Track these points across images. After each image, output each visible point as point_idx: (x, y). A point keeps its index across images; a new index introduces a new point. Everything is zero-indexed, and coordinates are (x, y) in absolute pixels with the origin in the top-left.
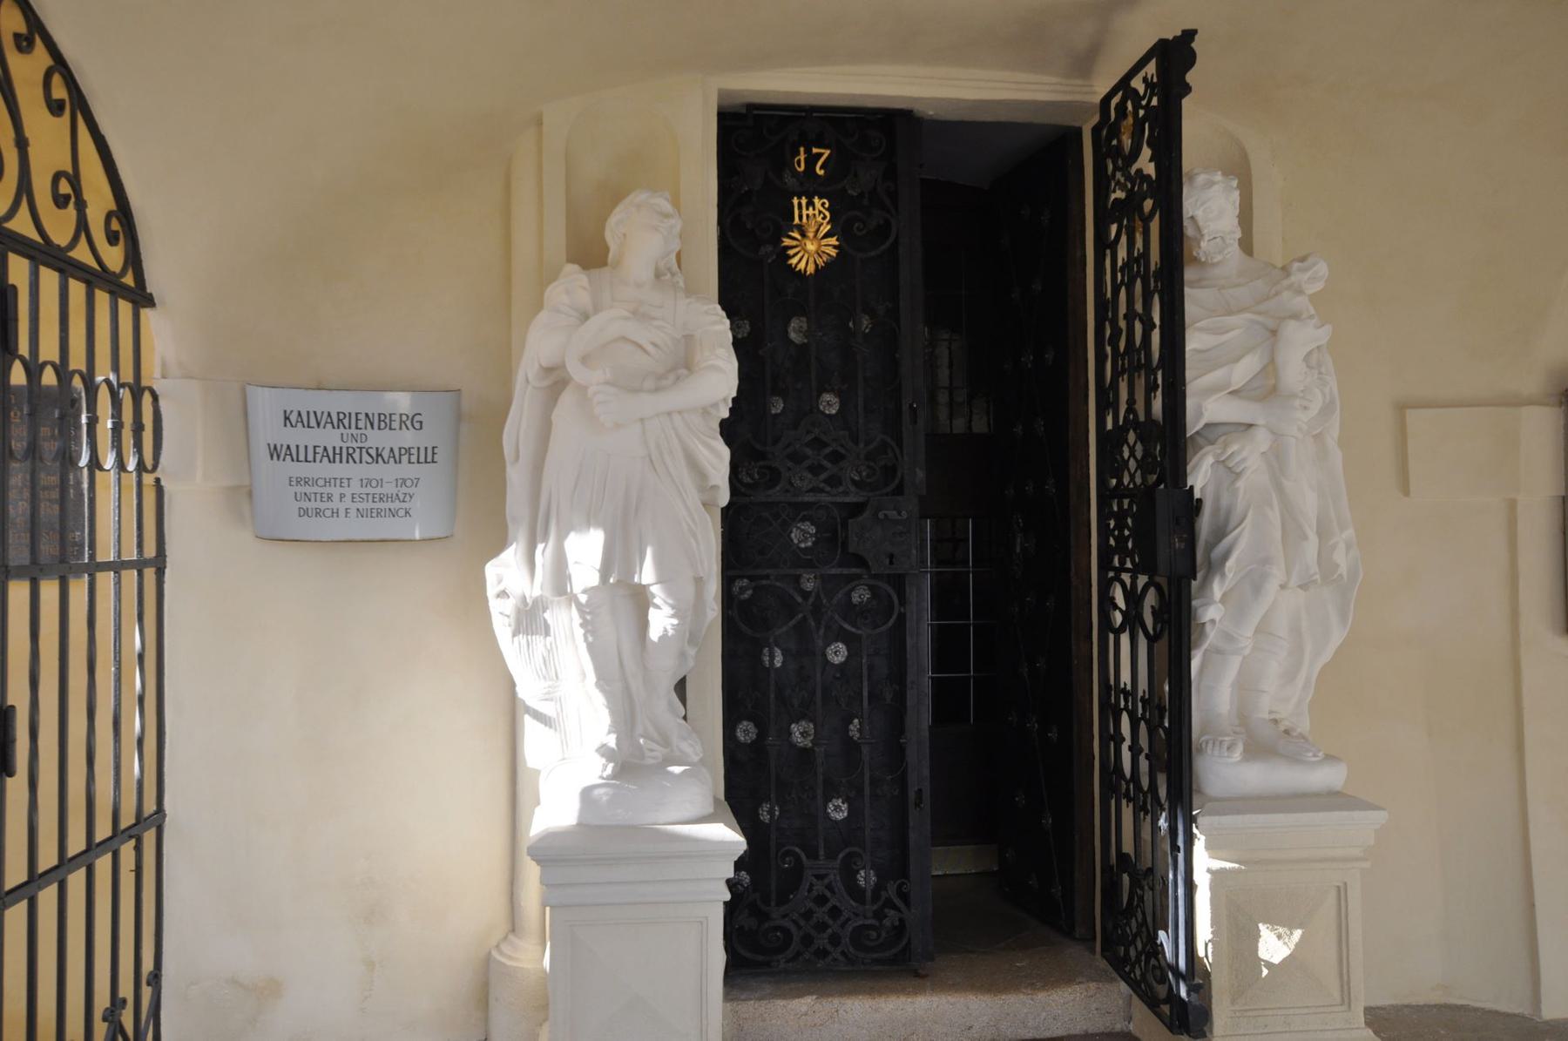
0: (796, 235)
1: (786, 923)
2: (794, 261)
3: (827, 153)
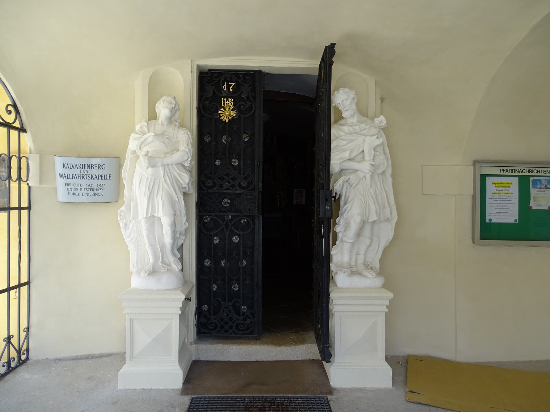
2: (222, 118)
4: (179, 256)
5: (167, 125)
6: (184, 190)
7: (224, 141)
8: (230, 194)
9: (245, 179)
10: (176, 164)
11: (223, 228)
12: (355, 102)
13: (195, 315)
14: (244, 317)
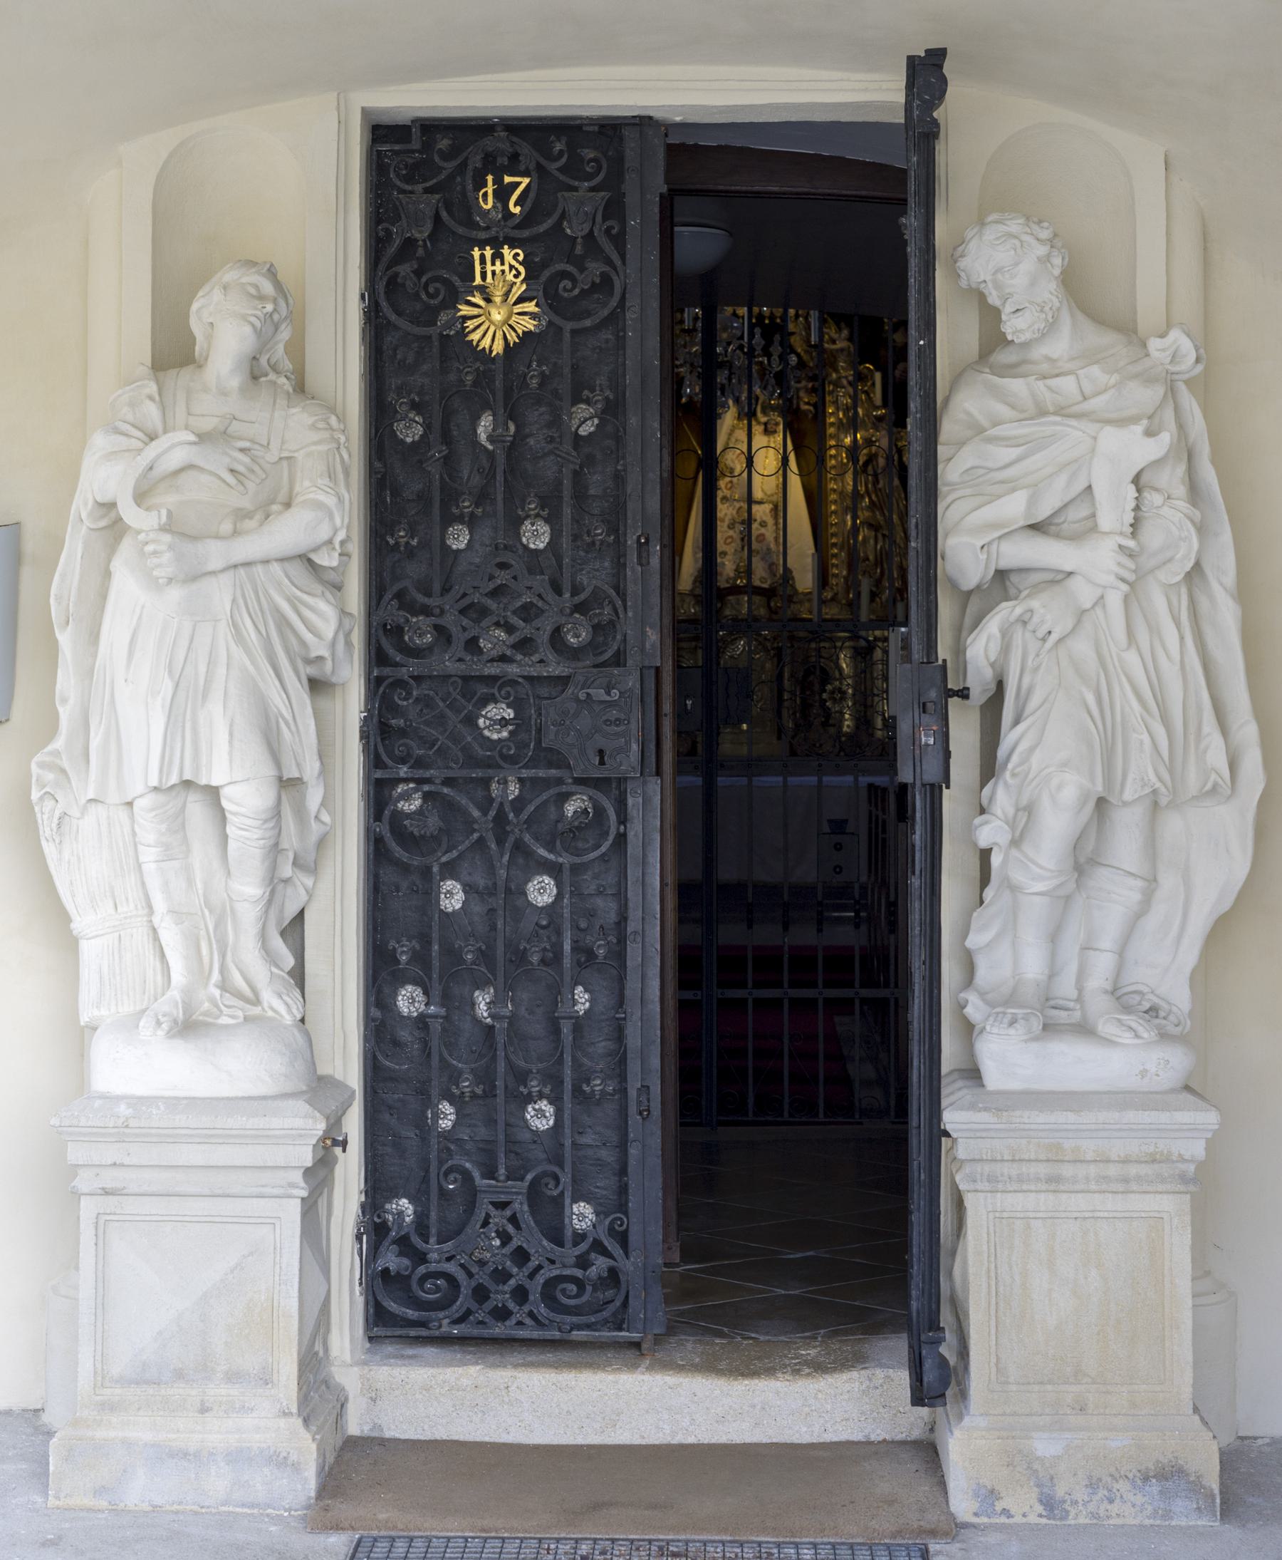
0: (477, 299)
1: (451, 1268)
2: (475, 337)
3: (526, 181)
4: (290, 962)
5: (243, 390)
6: (312, 671)
7: (483, 437)
8: (513, 683)
9: (581, 608)
10: (281, 560)
11: (481, 840)
12: (1057, 272)
13: (359, 1238)
14: (584, 1247)
